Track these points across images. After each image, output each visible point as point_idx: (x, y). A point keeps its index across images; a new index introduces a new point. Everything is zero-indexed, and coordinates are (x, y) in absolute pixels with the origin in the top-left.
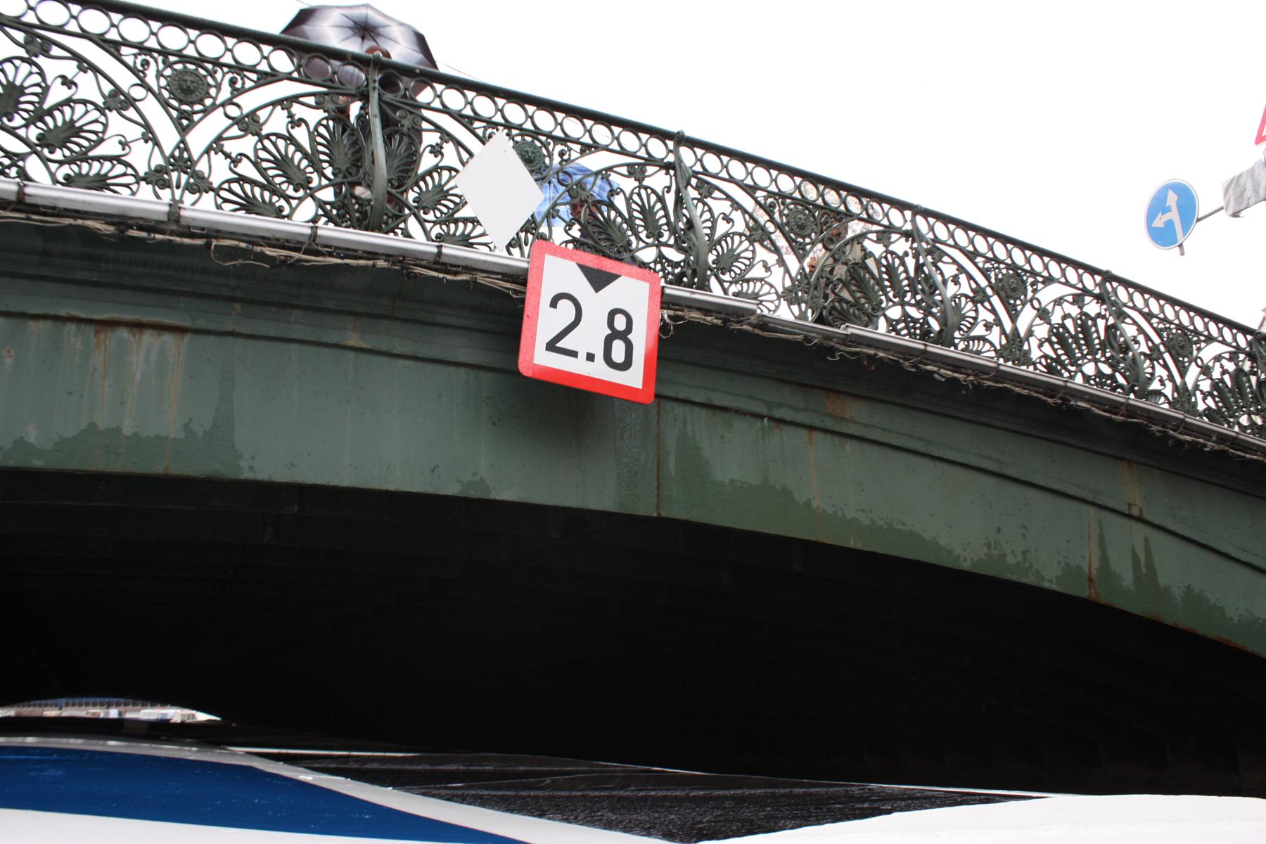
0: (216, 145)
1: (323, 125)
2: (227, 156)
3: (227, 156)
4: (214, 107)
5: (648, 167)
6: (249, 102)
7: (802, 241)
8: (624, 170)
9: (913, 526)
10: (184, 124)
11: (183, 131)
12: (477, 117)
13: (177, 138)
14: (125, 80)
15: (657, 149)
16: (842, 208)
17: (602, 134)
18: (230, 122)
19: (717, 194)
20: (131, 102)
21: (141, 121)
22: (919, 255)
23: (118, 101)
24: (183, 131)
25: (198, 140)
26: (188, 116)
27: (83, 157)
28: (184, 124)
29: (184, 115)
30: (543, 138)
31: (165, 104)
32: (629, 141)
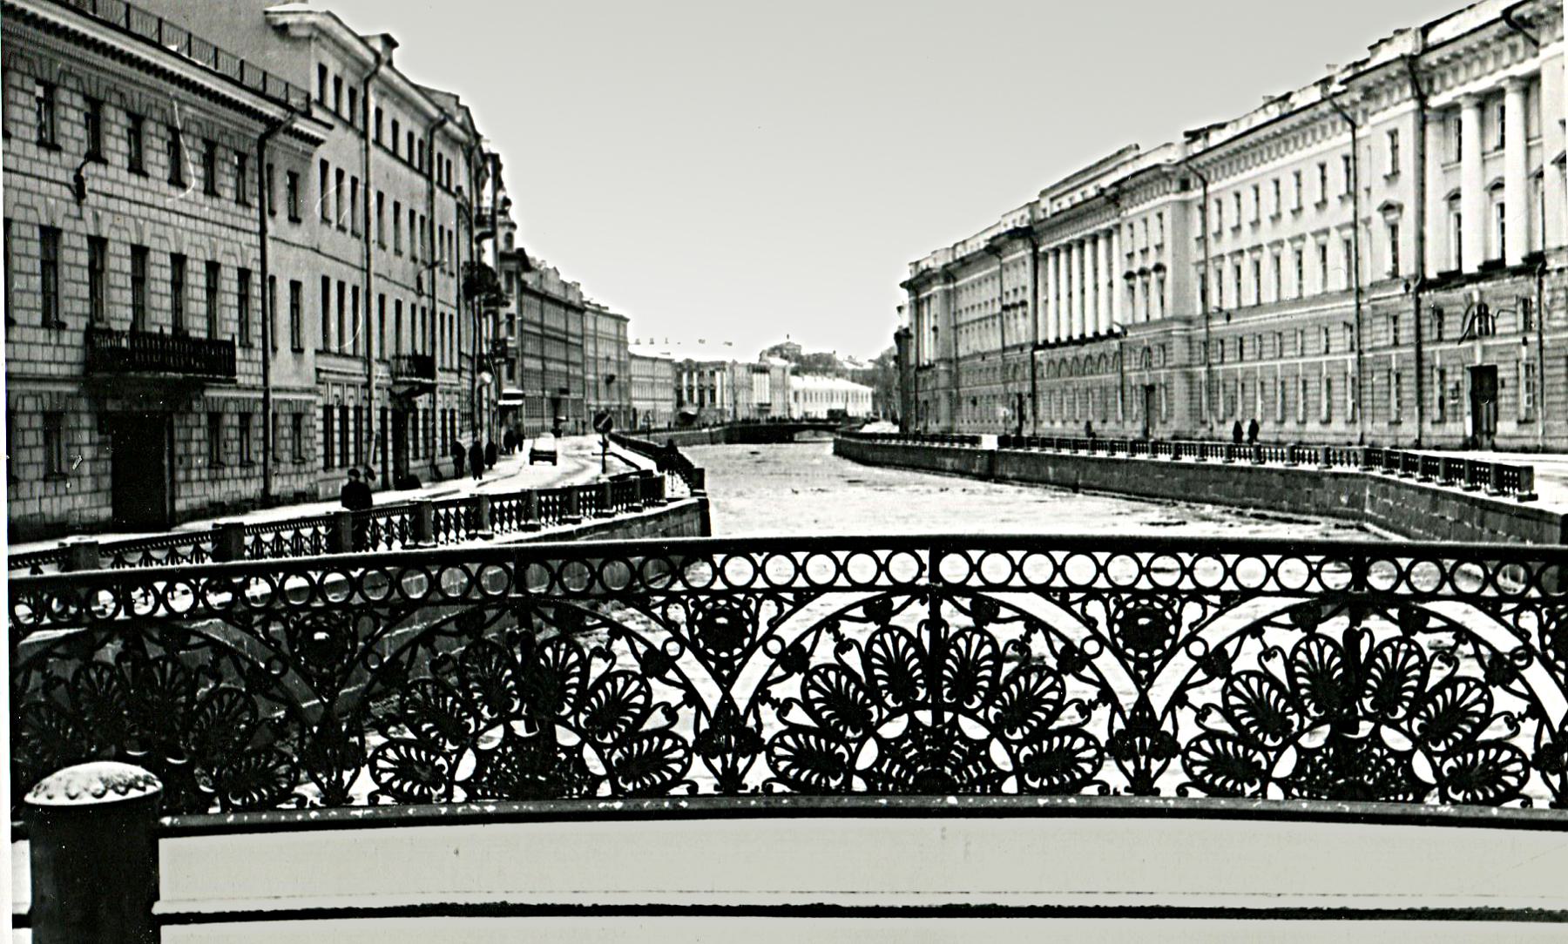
0: (1179, 699)
1: (1392, 647)
2: (1522, 717)
3: (1522, 717)
4: (1174, 650)
5: (894, 599)
6: (789, 631)
7: (589, 753)
8: (859, 612)
9: (900, 309)
10: (1144, 678)
11: (726, 683)
12: (1504, 597)
13: (720, 694)
14: (659, 637)
15: (904, 567)
16: (759, 560)
17: (821, 568)
18: (1194, 663)
19: (1004, 613)
20: (1087, 660)
21: (1096, 679)
22: (397, 800)
23: (657, 663)
24: (726, 683)
25: (742, 692)
26: (1147, 664)
27: (1470, 744)
28: (1144, 678)
29: (722, 663)
30: (741, 596)
31: (1121, 656)
32: (862, 567)
